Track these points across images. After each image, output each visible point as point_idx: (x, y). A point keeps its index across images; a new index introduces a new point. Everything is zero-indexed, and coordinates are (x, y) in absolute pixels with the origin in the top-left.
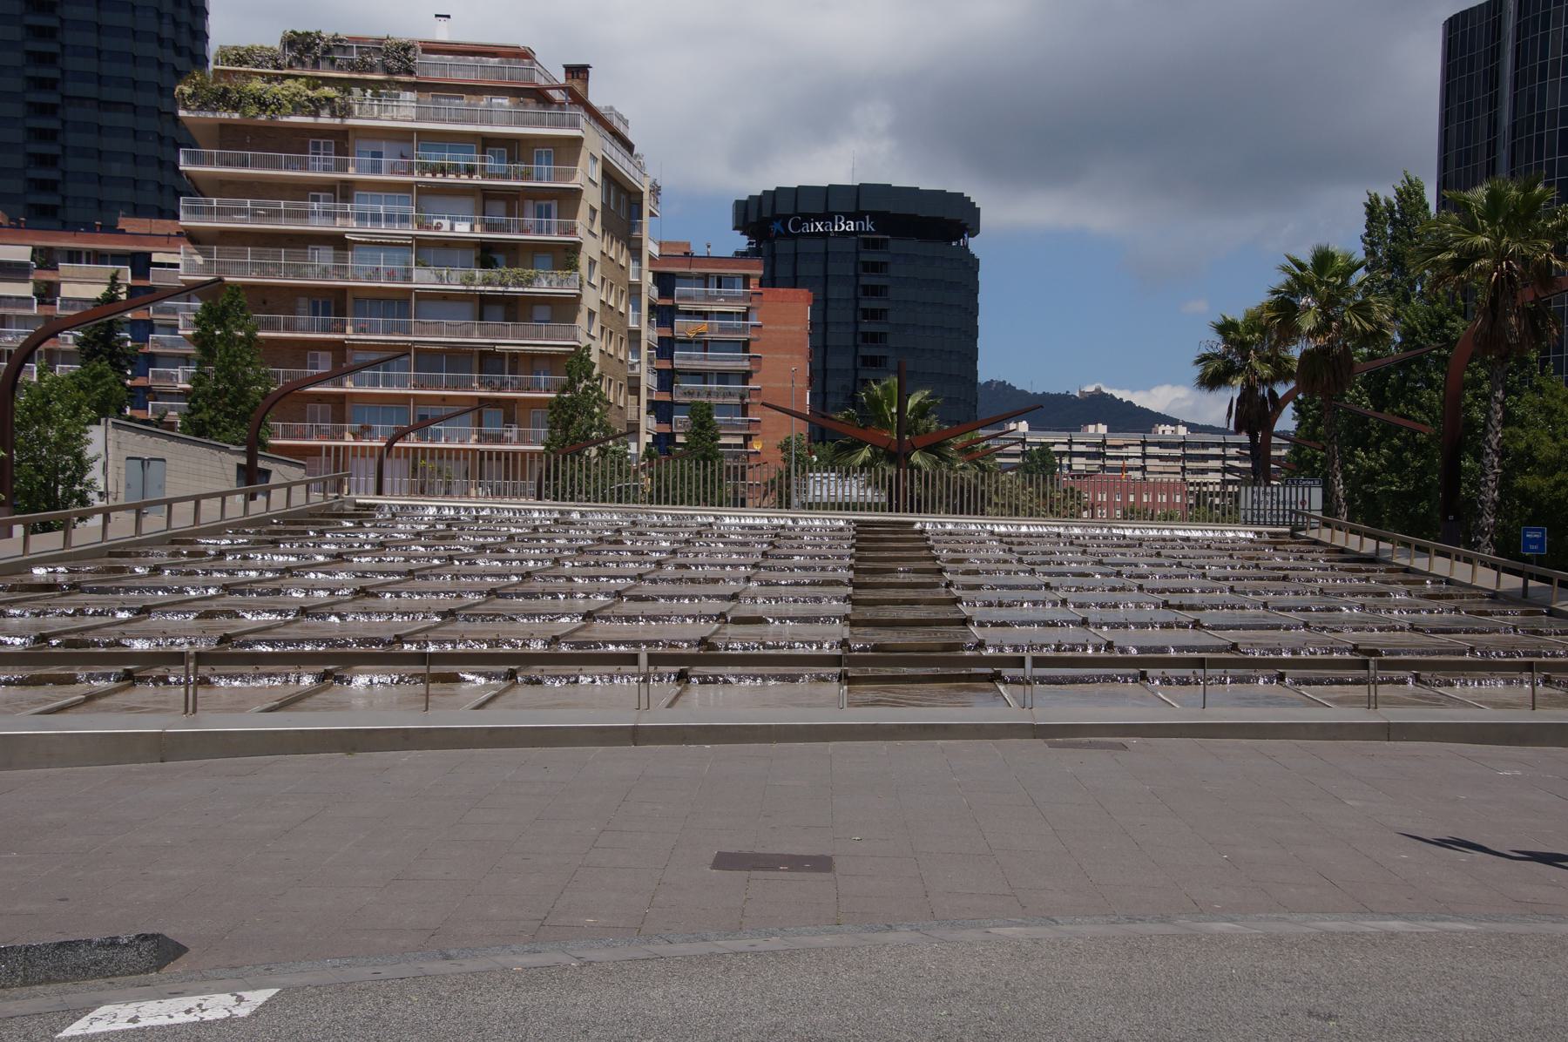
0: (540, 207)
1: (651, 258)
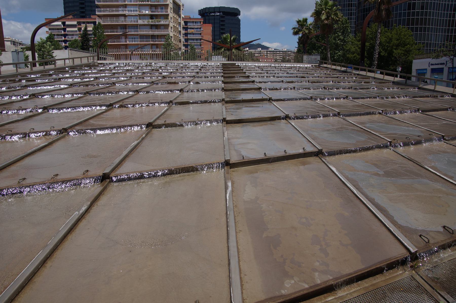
0: (161, 8)
1: (183, 18)
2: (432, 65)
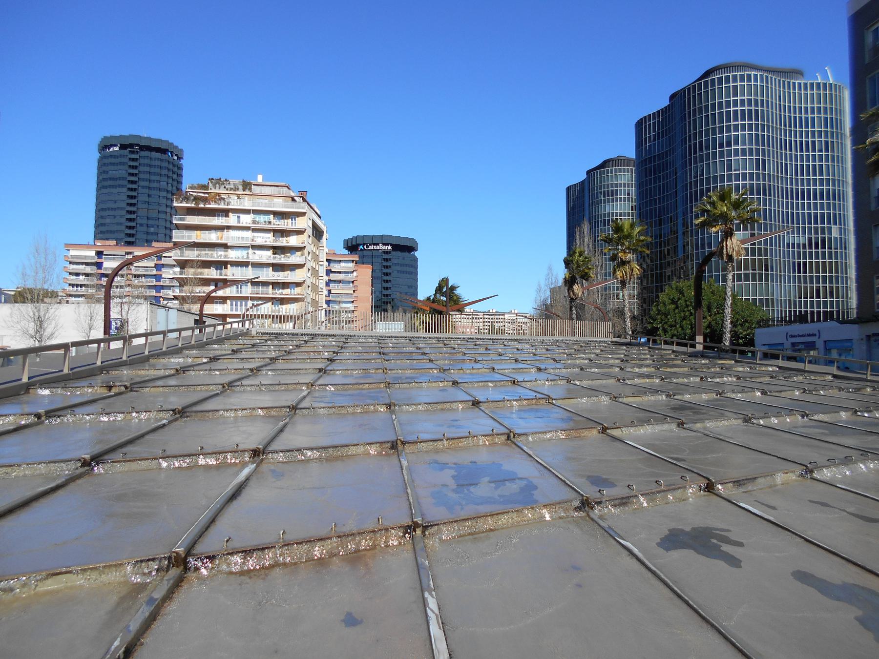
2: (792, 336)
